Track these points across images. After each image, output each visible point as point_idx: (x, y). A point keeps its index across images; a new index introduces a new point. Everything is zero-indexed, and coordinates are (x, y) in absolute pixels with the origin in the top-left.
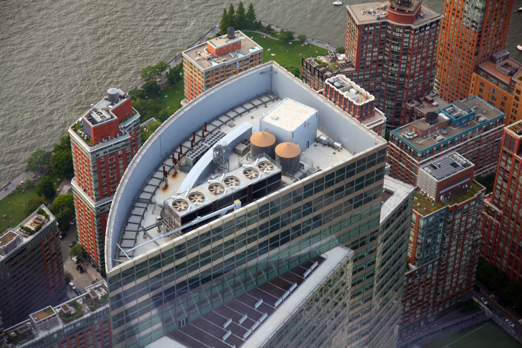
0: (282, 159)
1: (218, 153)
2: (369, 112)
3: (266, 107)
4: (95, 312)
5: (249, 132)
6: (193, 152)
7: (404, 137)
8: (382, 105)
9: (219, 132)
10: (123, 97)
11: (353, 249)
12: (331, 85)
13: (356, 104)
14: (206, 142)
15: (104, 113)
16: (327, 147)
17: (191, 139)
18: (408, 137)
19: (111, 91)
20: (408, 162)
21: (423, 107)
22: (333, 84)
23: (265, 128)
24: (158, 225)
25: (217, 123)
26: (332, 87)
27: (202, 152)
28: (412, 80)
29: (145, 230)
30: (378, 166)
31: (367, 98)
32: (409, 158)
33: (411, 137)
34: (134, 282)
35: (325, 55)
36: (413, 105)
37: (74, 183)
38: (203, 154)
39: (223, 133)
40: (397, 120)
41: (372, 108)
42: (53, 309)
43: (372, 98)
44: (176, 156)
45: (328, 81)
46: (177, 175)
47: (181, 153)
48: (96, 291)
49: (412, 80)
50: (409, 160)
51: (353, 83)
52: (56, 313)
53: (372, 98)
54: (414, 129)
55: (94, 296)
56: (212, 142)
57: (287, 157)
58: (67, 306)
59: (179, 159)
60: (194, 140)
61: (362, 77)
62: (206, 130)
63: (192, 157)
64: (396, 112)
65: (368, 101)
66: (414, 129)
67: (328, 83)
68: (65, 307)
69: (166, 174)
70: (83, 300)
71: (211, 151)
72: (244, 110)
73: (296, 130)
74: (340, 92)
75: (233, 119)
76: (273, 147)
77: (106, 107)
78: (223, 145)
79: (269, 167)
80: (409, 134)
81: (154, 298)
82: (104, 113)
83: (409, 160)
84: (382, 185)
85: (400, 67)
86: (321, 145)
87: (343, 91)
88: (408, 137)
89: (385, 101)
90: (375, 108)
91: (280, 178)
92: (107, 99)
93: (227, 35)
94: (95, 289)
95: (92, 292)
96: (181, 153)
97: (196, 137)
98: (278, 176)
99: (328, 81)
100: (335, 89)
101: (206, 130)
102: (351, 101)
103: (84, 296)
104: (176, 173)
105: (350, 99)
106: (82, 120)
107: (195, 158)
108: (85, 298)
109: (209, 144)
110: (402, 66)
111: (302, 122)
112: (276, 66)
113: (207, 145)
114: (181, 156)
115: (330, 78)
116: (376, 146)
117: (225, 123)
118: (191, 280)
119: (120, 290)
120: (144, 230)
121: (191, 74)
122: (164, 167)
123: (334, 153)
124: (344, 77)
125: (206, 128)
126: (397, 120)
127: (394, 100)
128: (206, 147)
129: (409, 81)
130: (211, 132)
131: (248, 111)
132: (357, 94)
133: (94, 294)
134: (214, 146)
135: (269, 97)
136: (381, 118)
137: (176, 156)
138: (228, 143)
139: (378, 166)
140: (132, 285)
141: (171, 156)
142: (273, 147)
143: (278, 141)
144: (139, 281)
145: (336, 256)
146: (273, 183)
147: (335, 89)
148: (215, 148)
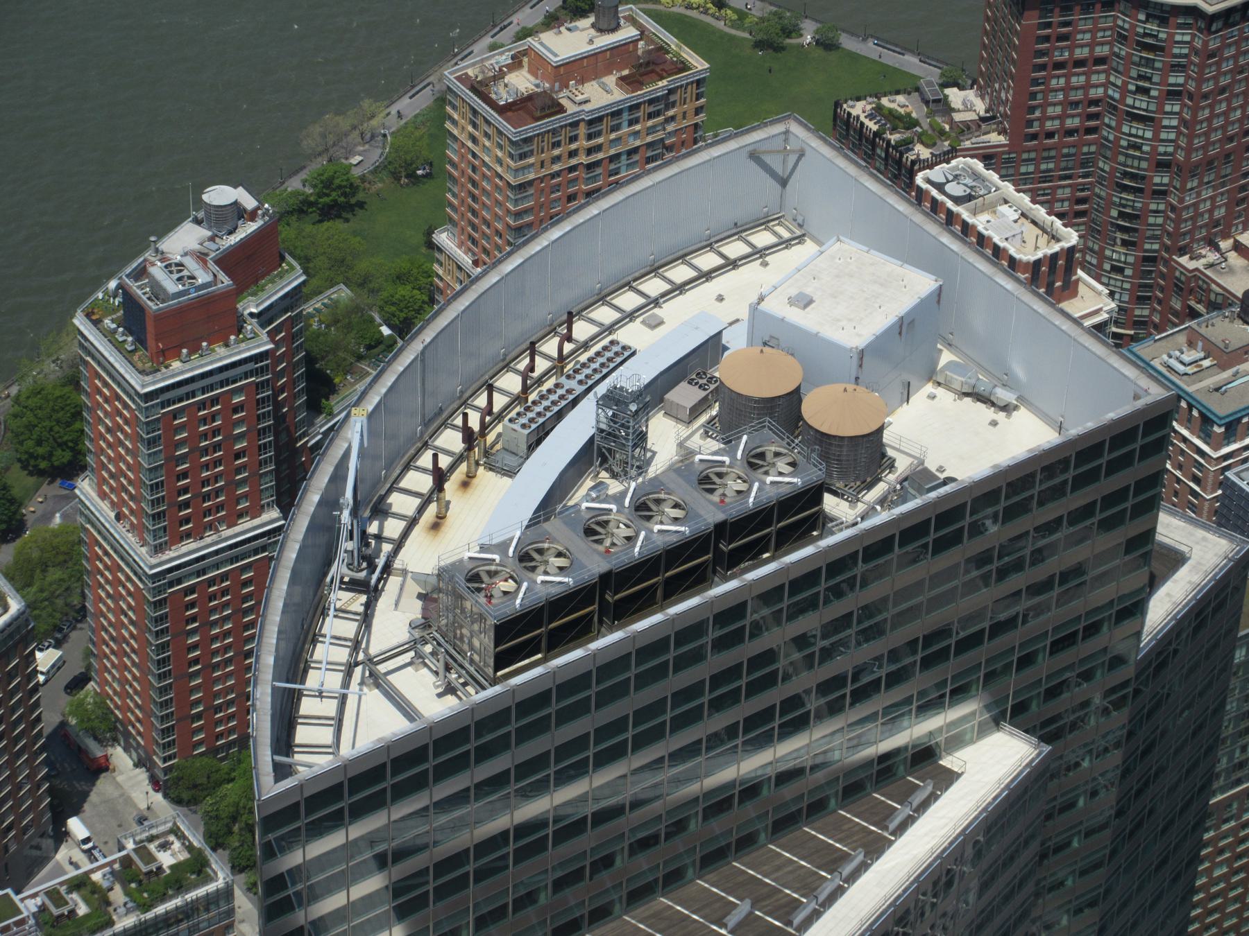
0: (823, 439)
1: (610, 413)
2: (1058, 284)
3: (765, 264)
4: (150, 915)
5: (713, 347)
6: (528, 409)
7: (1169, 368)
8: (1094, 261)
9: (612, 342)
10: (252, 216)
11: (1044, 739)
12: (934, 193)
13: (1017, 256)
14: (569, 377)
15: (192, 265)
16: (968, 400)
17: (523, 364)
18: (1181, 368)
19: (220, 195)
20: (1182, 452)
21: (1231, 271)
22: (940, 187)
23: (769, 336)
24: (413, 645)
25: (604, 314)
26: (940, 197)
27: (556, 409)
28: (1195, 183)
29: (370, 661)
30: (1140, 470)
31: (1055, 238)
32: (1185, 440)
33: (1190, 370)
34: (343, 832)
35: (909, 94)
36: (1199, 264)
37: (85, 487)
38: (560, 416)
39: (624, 348)
40: (1141, 312)
41: (1069, 270)
42: (16, 899)
43: (1071, 237)
44: (474, 422)
45: (929, 181)
46: (475, 481)
47: (489, 410)
48: (152, 847)
49: (1195, 183)
50: (1182, 446)
51: (1008, 188)
52: (25, 914)
53: (1071, 237)
54: (1200, 344)
55: (146, 864)
56: (588, 377)
57: (833, 432)
58: (63, 889)
59: (484, 427)
60: (531, 368)
61: (1031, 168)
62: (569, 338)
63: (524, 426)
64: (1141, 286)
65: (1056, 248)
66: (1200, 344)
67: (925, 186)
68: (53, 894)
69: (440, 477)
70: (113, 873)
71: (588, 407)
72: (692, 274)
73: (867, 346)
74: (965, 215)
75: (656, 302)
76: (795, 397)
77: (198, 247)
78: (632, 386)
79: (782, 466)
80: (1187, 358)
81: (397, 889)
82: (192, 265)
83: (1182, 446)
84: (1152, 531)
85: (1156, 137)
86: (951, 396)
87: (974, 213)
88: (1181, 368)
89: (1102, 249)
90: (1080, 272)
91: (819, 500)
92: (198, 222)
93: (592, 19)
94: (151, 839)
95: (141, 850)
96: (489, 410)
97: (538, 359)
98: (812, 495)
99: (929, 181)
100: (950, 204)
101: (569, 338)
102: (1002, 244)
103: (114, 861)
104: (470, 476)
105: (996, 240)
106: (120, 286)
107: (534, 426)
108: (117, 866)
109: (580, 382)
110: (1163, 136)
111: (891, 319)
112: (795, 128)
113: (572, 384)
114: (488, 418)
115: (931, 167)
116: (1140, 404)
117: (630, 316)
118: (523, 830)
119: (295, 858)
120: (370, 660)
121: (470, 144)
122: (435, 456)
123: (994, 423)
124: (979, 166)
125: (570, 329)
126: (1141, 312)
127: (1133, 244)
128: (569, 391)
129: (1184, 184)
130: (586, 346)
131: (707, 276)
132: (1017, 221)
133: (150, 858)
134: (601, 389)
135: (775, 234)
136: (1093, 299)
137: (474, 422)
138: (646, 378)
139: (1140, 470)
140: (333, 841)
141: (459, 421)
142: (795, 397)
143: (815, 376)
144: (358, 830)
145: (991, 762)
146: (798, 515)
147: (950, 204)
148: (604, 397)
